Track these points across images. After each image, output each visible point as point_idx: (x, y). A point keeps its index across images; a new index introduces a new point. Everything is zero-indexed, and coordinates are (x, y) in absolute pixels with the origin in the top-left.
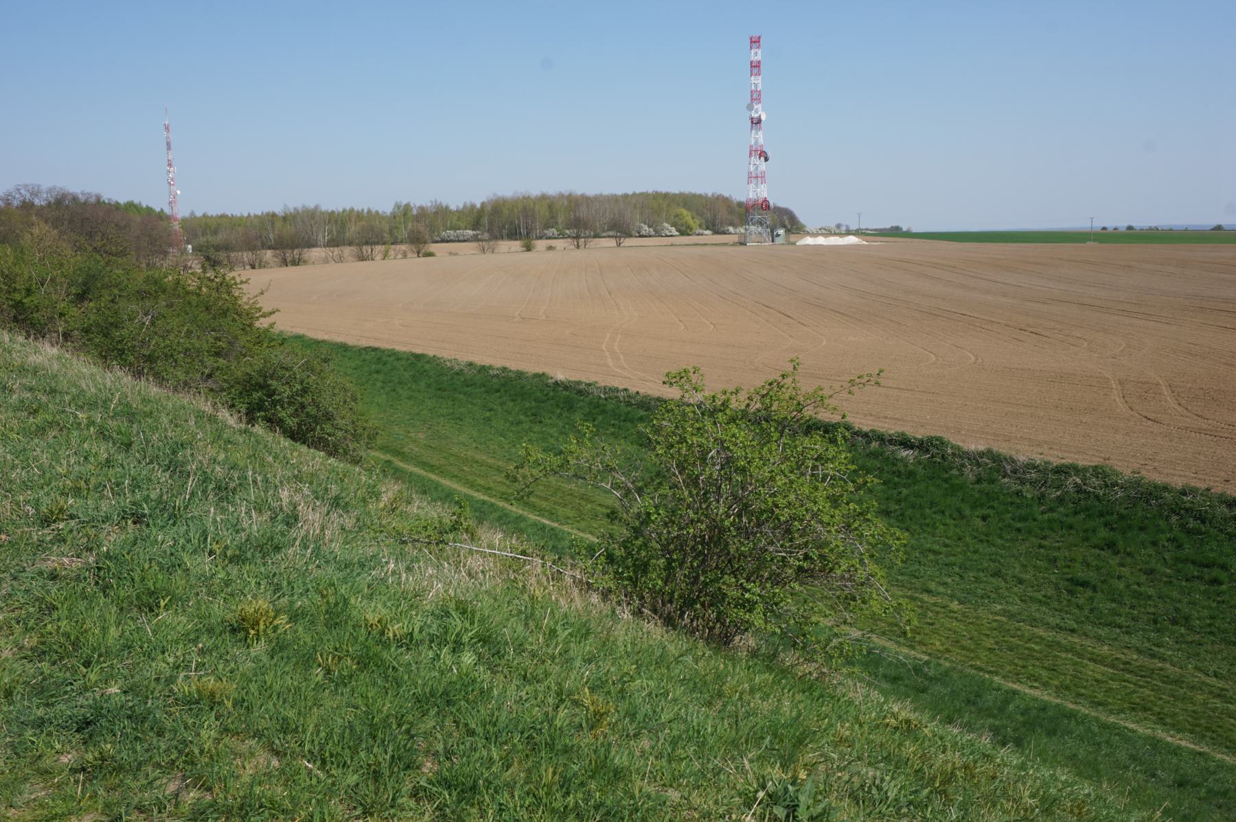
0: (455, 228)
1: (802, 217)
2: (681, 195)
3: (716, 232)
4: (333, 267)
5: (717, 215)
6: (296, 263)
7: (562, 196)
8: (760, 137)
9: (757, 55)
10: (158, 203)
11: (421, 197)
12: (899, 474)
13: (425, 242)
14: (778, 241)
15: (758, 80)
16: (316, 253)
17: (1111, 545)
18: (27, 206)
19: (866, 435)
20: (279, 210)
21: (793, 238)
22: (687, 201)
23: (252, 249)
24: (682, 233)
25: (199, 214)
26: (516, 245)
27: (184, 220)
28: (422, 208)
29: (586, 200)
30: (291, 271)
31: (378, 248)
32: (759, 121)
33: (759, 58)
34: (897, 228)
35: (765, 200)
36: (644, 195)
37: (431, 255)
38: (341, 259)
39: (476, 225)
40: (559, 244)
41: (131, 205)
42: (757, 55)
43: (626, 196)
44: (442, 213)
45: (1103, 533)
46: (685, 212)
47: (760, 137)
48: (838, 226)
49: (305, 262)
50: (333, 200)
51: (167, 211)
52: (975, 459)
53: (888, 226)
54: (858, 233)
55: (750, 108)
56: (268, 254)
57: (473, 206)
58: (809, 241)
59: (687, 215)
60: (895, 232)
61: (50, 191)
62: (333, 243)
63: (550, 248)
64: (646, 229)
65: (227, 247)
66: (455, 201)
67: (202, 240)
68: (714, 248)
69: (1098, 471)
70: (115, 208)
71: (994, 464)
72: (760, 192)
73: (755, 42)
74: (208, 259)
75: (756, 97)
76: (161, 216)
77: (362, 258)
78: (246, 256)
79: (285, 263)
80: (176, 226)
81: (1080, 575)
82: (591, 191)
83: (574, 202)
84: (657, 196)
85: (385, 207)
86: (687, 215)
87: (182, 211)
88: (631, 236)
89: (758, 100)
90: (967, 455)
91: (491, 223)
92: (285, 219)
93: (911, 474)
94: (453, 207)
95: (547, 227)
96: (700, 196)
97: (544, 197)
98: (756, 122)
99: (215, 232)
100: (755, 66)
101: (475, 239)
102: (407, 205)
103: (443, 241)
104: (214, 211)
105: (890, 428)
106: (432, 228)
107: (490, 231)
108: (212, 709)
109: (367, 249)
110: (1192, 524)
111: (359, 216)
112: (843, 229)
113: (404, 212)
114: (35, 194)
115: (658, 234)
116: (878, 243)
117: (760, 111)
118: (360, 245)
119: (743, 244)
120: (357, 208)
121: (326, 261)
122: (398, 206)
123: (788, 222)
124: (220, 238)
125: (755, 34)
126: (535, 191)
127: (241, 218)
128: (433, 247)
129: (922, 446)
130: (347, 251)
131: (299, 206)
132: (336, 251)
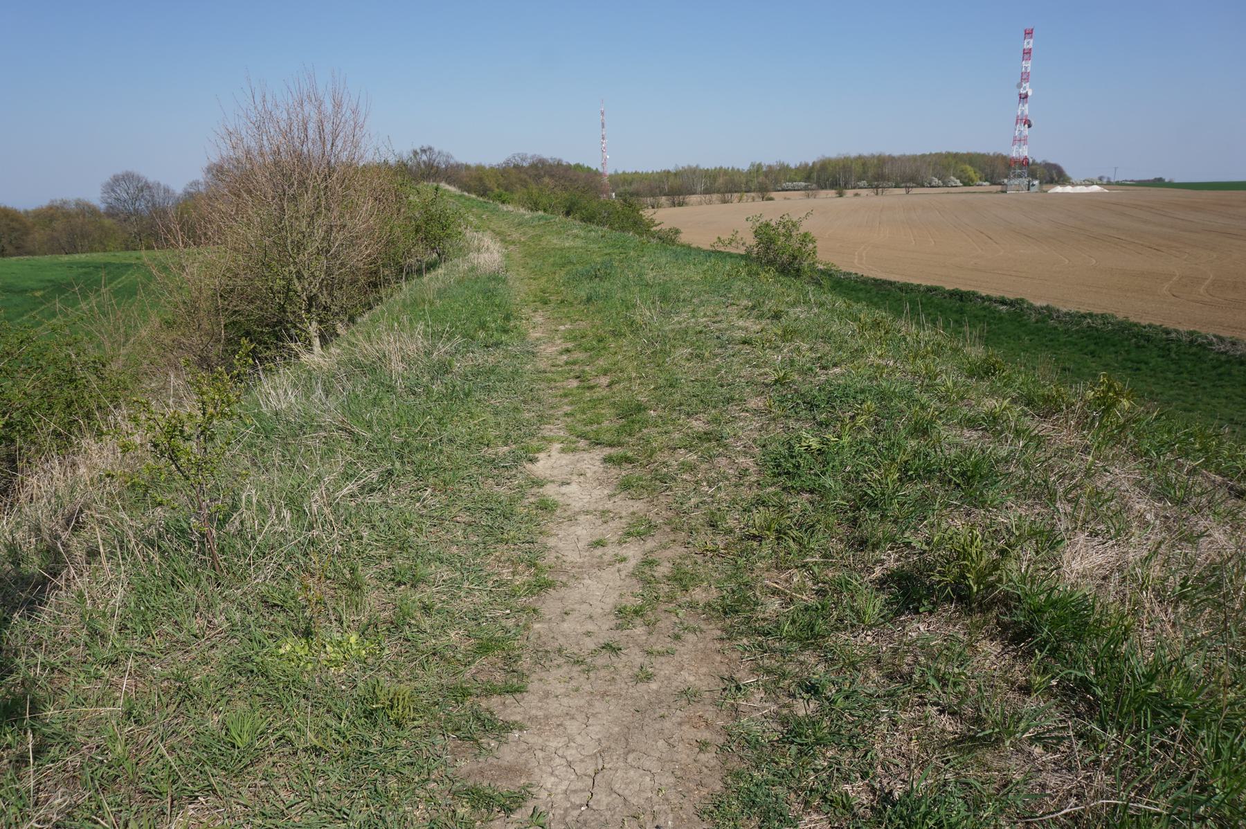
0: (792, 181)
1: (1069, 172)
2: (968, 154)
3: (993, 183)
4: (704, 207)
5: (995, 170)
6: (680, 205)
7: (873, 157)
8: (1025, 109)
9: (1029, 44)
10: (594, 165)
11: (770, 158)
12: (994, 318)
13: (768, 191)
14: (1033, 189)
15: (1028, 65)
16: (694, 198)
17: (1092, 353)
18: (516, 167)
19: (982, 298)
20: (672, 168)
21: (1045, 187)
22: (971, 159)
23: (653, 196)
24: (965, 184)
25: (620, 172)
26: (832, 193)
27: (611, 176)
28: (770, 167)
29: (892, 159)
30: (677, 210)
31: (735, 195)
32: (1026, 96)
33: (1030, 46)
34: (1160, 180)
35: (1026, 158)
36: (939, 155)
37: (771, 199)
38: (710, 202)
39: (808, 178)
40: (864, 192)
41: (578, 166)
42: (1029, 44)
43: (923, 156)
44: (784, 169)
45: (1092, 347)
46: (969, 168)
47: (1025, 109)
48: (1100, 179)
49: (687, 204)
50: (708, 161)
51: (601, 170)
52: (1038, 310)
53: (1152, 178)
54: (1100, 182)
55: (1019, 86)
56: (663, 199)
57: (807, 165)
58: (1069, 189)
59: (970, 171)
60: (1158, 183)
61: (533, 157)
62: (707, 191)
63: (856, 195)
64: (936, 181)
65: (637, 194)
66: (793, 162)
67: (621, 189)
68: (1189, 192)
69: (1103, 316)
70: (568, 168)
71: (1048, 313)
72: (1023, 152)
73: (1029, 33)
74: (625, 201)
75: (1025, 77)
76: (596, 173)
77: (724, 202)
78: (649, 200)
79: (674, 205)
80: (606, 180)
81: (1067, 365)
82: (896, 153)
83: (882, 161)
84: (948, 155)
85: (745, 166)
86: (970, 171)
87: (609, 170)
88: (923, 186)
89: (1027, 80)
90: (1031, 307)
91: (819, 177)
92: (675, 174)
93: (1001, 319)
94: (792, 166)
95: (860, 179)
96: (979, 155)
97: (860, 157)
98: (1024, 97)
99: (631, 184)
100: (1027, 53)
101: (806, 188)
102: (760, 165)
103: (783, 190)
104: (630, 169)
105: (995, 294)
106: (777, 181)
107: (818, 183)
108: (613, 246)
109: (728, 196)
110: (1142, 342)
111: (726, 172)
112: (1105, 181)
113: (757, 169)
114: (524, 160)
115: (945, 185)
116: (1118, 191)
117: (1028, 89)
118: (723, 193)
119: (1004, 192)
120: (725, 166)
121: (700, 203)
122: (753, 165)
123: (1054, 175)
124: (635, 186)
125: (1029, 27)
126: (853, 152)
127: (647, 174)
128: (773, 194)
129: (1012, 304)
130: (715, 196)
131: (686, 166)
132: (708, 196)
